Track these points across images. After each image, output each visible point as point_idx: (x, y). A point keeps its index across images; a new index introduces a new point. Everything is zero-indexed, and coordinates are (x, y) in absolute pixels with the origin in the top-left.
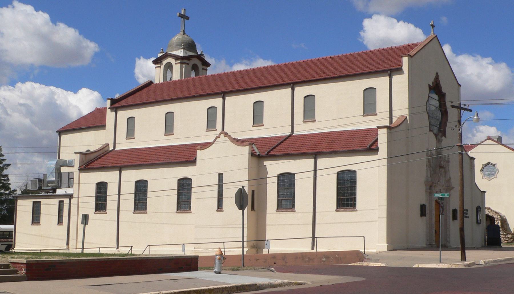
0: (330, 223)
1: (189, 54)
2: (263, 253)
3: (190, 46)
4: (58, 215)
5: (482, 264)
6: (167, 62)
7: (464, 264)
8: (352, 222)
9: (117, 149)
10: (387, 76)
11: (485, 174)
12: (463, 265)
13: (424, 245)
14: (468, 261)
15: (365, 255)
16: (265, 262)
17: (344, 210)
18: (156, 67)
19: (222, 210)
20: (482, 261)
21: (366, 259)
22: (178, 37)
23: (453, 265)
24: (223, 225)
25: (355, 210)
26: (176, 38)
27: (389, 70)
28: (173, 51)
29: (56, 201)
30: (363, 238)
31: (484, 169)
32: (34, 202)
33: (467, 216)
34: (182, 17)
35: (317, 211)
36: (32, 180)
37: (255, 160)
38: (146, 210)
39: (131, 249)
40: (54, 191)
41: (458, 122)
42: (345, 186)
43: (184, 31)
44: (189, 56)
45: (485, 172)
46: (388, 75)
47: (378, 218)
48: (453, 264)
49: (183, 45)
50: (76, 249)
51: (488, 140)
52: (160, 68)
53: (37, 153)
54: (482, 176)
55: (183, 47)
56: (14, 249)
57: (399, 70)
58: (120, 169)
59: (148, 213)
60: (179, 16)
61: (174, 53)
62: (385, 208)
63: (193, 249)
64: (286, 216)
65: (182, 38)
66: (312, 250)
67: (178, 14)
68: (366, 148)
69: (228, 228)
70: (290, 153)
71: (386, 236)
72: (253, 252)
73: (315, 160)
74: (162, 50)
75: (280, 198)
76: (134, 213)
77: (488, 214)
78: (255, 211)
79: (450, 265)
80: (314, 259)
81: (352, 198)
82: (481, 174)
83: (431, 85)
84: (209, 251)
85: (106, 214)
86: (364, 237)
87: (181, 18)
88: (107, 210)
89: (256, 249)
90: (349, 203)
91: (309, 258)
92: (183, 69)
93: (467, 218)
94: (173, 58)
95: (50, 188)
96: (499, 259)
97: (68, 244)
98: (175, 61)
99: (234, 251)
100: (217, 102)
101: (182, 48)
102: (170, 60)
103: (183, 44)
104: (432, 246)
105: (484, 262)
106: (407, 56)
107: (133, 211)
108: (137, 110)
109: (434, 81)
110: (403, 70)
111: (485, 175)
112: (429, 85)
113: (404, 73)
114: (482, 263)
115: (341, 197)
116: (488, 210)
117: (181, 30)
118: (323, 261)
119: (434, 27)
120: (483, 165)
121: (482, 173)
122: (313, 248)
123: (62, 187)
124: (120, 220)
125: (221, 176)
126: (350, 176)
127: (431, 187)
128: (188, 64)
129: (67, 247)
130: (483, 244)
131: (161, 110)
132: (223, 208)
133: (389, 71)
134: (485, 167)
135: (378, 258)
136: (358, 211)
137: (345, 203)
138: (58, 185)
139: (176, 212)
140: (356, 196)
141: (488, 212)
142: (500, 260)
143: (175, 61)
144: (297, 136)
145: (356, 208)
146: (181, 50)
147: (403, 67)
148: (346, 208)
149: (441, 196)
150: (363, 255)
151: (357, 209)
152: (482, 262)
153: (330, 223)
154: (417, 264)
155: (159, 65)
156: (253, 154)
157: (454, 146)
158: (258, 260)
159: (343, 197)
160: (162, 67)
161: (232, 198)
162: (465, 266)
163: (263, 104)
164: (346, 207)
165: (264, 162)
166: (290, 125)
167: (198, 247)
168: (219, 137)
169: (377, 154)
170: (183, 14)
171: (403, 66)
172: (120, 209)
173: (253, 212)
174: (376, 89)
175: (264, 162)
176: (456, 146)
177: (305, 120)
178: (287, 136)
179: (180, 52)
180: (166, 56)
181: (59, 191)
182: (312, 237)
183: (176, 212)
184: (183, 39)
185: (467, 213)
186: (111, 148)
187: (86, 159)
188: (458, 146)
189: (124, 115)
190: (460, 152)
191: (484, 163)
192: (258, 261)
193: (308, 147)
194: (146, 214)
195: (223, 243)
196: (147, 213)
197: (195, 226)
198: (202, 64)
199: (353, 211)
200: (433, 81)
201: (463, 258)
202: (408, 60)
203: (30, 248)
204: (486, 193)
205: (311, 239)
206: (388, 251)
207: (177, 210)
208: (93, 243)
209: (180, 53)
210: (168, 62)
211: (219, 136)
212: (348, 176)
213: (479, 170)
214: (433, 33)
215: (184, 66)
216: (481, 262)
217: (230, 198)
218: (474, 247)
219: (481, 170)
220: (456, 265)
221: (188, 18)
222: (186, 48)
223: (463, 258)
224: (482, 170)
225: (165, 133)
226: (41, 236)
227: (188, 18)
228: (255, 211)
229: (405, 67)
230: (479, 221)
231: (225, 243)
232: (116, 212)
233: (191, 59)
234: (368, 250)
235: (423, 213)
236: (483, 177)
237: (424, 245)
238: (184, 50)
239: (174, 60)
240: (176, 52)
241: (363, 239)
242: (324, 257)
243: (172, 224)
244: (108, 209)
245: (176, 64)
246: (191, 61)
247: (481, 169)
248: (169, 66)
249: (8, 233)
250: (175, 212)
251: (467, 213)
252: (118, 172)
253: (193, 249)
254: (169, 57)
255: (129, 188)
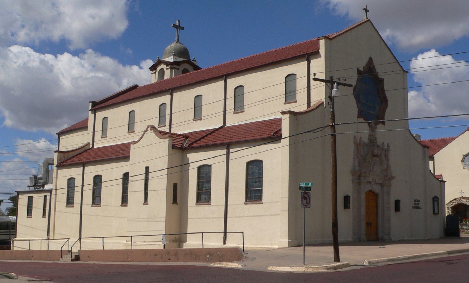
0: (240, 217)
1: (180, 59)
2: (184, 248)
3: (183, 53)
4: (43, 208)
5: (366, 264)
6: (160, 69)
7: (326, 266)
8: (258, 216)
9: (95, 147)
10: (305, 61)
11: (466, 164)
12: (326, 268)
13: (350, 239)
14: (341, 262)
15: (243, 253)
16: (161, 258)
17: (251, 203)
18: (152, 74)
19: (147, 204)
20: (366, 261)
21: (243, 257)
22: (172, 46)
23: (310, 268)
24: (148, 218)
25: (261, 202)
26: (170, 46)
27: (306, 54)
28: (166, 58)
29: (42, 195)
30: (242, 233)
31: (465, 160)
32: (29, 197)
33: (419, 207)
34: (177, 28)
35: (229, 204)
36: (31, 177)
37: (177, 154)
38: (100, 204)
39: (69, 240)
40: (43, 186)
41: (329, 98)
42: (254, 177)
43: (178, 40)
44: (179, 61)
45: (466, 162)
46: (306, 60)
47: (281, 211)
48: (310, 267)
49: (174, 52)
50: (54, 239)
51: (468, 131)
52: (155, 74)
53: (15, 153)
54: (463, 167)
55: (173, 53)
56: (16, 238)
57: (316, 54)
58: (84, 165)
59: (101, 206)
60: (173, 27)
61: (166, 60)
62: (287, 200)
63: (125, 242)
64: (204, 209)
65: (174, 46)
66: (223, 245)
67: (172, 25)
68: (271, 135)
69: (151, 221)
70: (207, 144)
71: (287, 231)
72: (174, 246)
73: (228, 151)
74: (159, 58)
75: (200, 191)
76: (92, 207)
77: (466, 204)
78: (178, 204)
79: (306, 268)
80: (200, 255)
81: (259, 189)
82: (462, 164)
83: (362, 69)
84: (136, 245)
85: (74, 208)
86: (243, 233)
87: (176, 28)
88: (74, 204)
89: (178, 243)
90: (254, 195)
91: (196, 254)
92: (172, 73)
93: (419, 208)
94: (164, 64)
95: (41, 184)
96: (400, 257)
97: (48, 235)
98: (167, 67)
99: (154, 245)
100: (166, 99)
101: (173, 55)
102: (163, 66)
103: (174, 51)
104: (360, 240)
105: (369, 262)
106: (324, 38)
107: (91, 205)
108: (109, 110)
109: (366, 65)
110: (320, 53)
111: (465, 165)
112: (358, 69)
113: (321, 57)
114: (366, 263)
115: (250, 189)
116: (466, 200)
117: (176, 40)
118: (208, 258)
119: (368, 11)
120: (464, 155)
121: (463, 164)
122: (225, 243)
123: (49, 183)
124: (83, 213)
125: (147, 168)
126: (258, 166)
127: (360, 176)
128: (178, 69)
129: (47, 238)
130: (443, 235)
131: (126, 109)
132: (148, 202)
133: (307, 55)
134: (466, 158)
135: (255, 257)
136: (264, 203)
137: (254, 195)
138: (47, 181)
139: (121, 206)
140: (262, 188)
141: (467, 201)
142: (401, 258)
143: (167, 67)
144: (228, 127)
145: (262, 201)
146: (172, 57)
147: (320, 50)
148: (254, 201)
149: (305, 186)
150: (241, 253)
151: (263, 201)
152: (366, 263)
153: (240, 217)
154: (270, 267)
155: (155, 72)
156: (173, 147)
157: (325, 127)
158: (156, 255)
159: (251, 189)
160: (157, 73)
161: (155, 191)
162: (328, 269)
163: (202, 98)
164: (254, 199)
165: (187, 155)
166: (169, 114)
167: (129, 240)
168: (147, 130)
169: (280, 143)
170: (177, 25)
171: (320, 49)
172: (83, 203)
173: (175, 205)
174: (296, 75)
175: (187, 155)
176: (328, 126)
177: (236, 111)
178: (216, 129)
179: (171, 58)
180: (159, 62)
181: (47, 187)
182: (224, 231)
183: (121, 206)
184: (176, 47)
185: (419, 204)
186: (91, 147)
187: (64, 157)
188: (330, 127)
189: (100, 115)
190: (332, 133)
191: (465, 154)
192: (156, 256)
193: (195, 137)
194: (100, 208)
195: (131, 237)
196: (100, 206)
197: (128, 219)
198: (193, 69)
199: (259, 204)
200: (365, 66)
201: (337, 258)
202: (325, 43)
203: (26, 238)
204: (445, 183)
205: (223, 233)
206: (289, 247)
207: (122, 204)
208: (64, 235)
209: (171, 59)
210: (161, 68)
211: (146, 130)
212: (256, 166)
213: (460, 160)
214: (366, 17)
215: (174, 71)
216: (365, 262)
217: (153, 191)
218: (428, 238)
219: (462, 161)
220: (314, 267)
221: (183, 28)
222: (176, 55)
223: (337, 258)
224: (463, 160)
225: (129, 131)
226: (32, 228)
227: (183, 28)
228: (178, 204)
229: (322, 51)
230: (436, 211)
231: (132, 237)
232: (80, 205)
233: (181, 65)
234: (273, 245)
235: (397, 203)
236: (464, 167)
237: (350, 239)
238: (175, 57)
239: (165, 66)
240: (168, 59)
241: (242, 235)
242: (208, 254)
243: (118, 217)
244: (75, 203)
245: (167, 69)
246: (180, 66)
247: (462, 159)
248: (162, 71)
249: (13, 224)
250: (120, 206)
251: (419, 204)
252: (82, 168)
253: (125, 242)
254: (162, 63)
255: (89, 180)
